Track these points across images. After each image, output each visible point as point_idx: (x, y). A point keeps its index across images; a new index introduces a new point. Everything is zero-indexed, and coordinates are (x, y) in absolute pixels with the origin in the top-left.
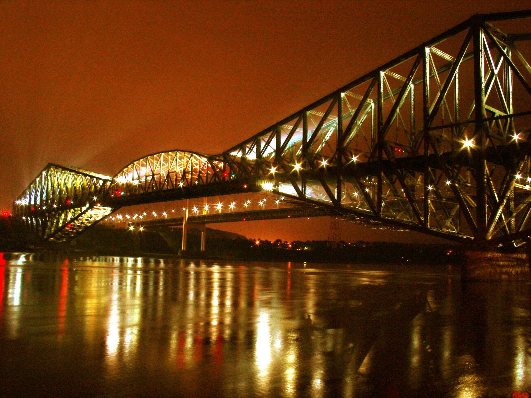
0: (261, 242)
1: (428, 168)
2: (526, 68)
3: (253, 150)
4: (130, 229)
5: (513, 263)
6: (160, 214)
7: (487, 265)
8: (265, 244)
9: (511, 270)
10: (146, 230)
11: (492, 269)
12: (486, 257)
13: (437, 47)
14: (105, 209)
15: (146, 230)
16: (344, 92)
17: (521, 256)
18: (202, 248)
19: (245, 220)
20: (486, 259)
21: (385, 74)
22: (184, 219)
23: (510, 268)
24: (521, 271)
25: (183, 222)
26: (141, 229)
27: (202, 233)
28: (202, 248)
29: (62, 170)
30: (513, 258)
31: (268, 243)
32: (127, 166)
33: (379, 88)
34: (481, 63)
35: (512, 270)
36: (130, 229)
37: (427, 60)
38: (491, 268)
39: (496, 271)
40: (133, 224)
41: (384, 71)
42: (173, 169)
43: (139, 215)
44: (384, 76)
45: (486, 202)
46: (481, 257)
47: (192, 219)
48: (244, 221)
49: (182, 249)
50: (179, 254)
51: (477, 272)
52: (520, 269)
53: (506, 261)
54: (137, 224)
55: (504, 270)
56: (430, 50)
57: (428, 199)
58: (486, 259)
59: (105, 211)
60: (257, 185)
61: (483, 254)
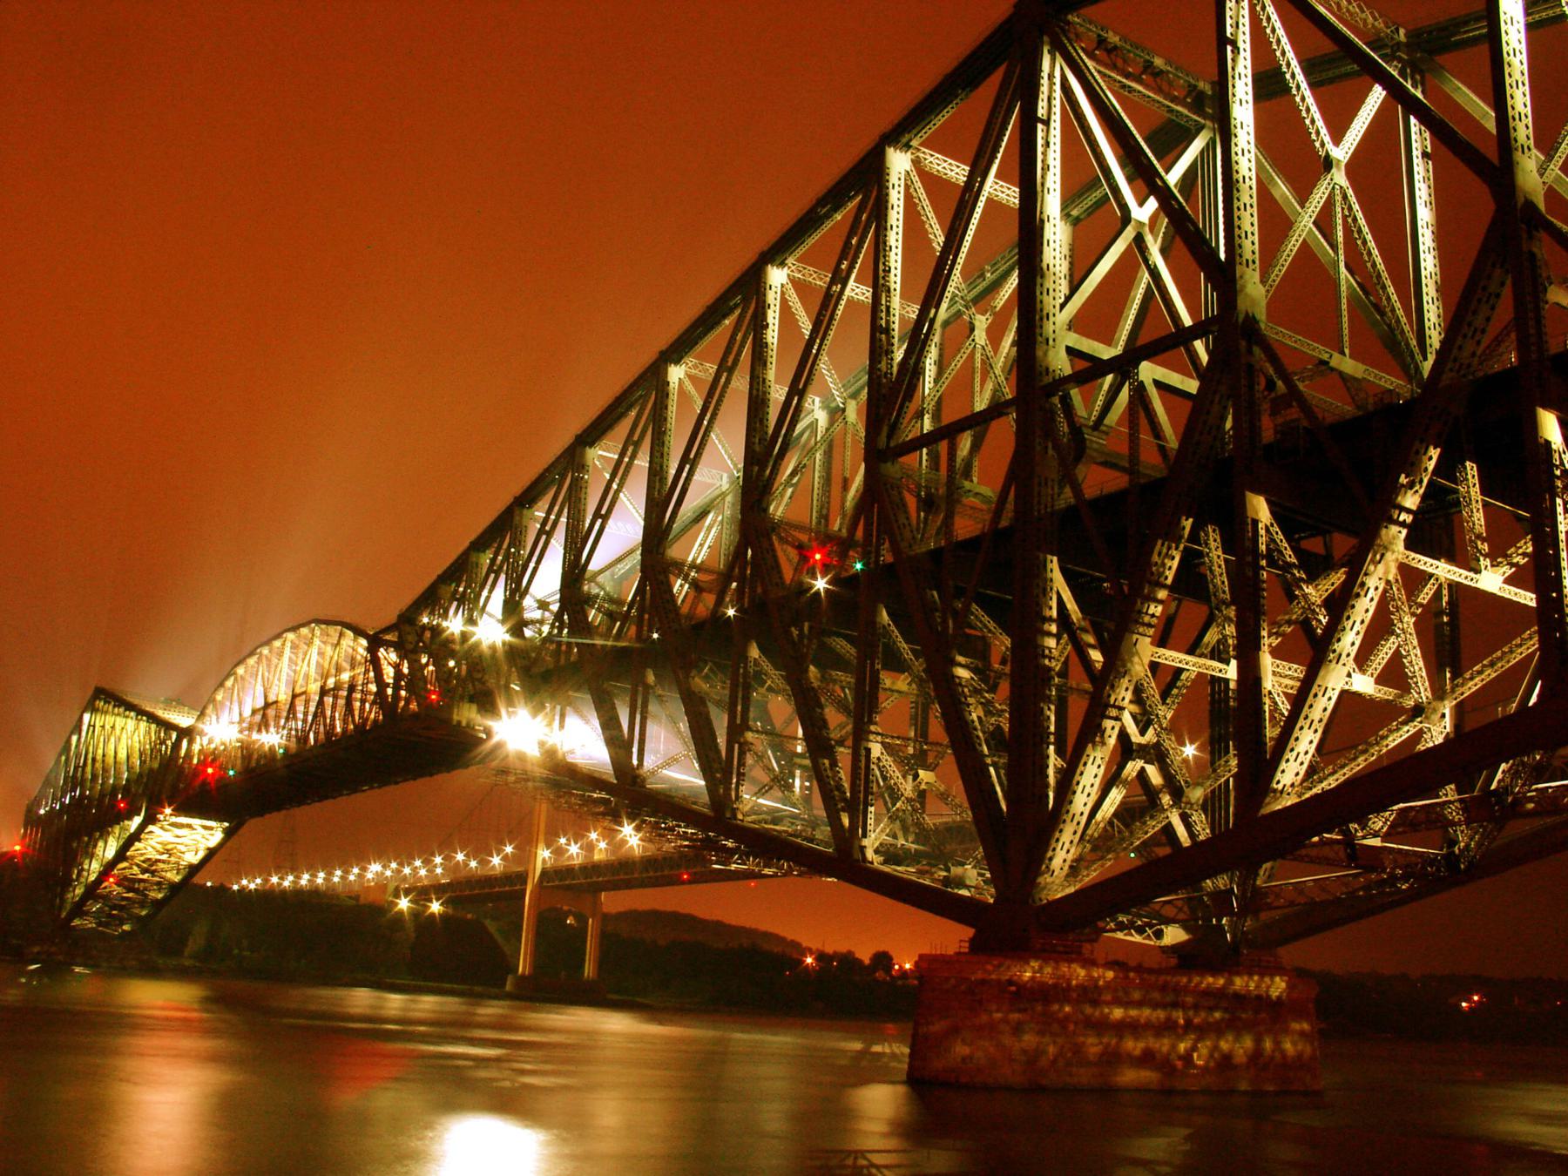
0: (821, 957)
1: (874, 613)
2: (1272, 195)
3: (488, 608)
4: (400, 907)
5: (1203, 1014)
6: (483, 862)
7: (1015, 1016)
8: (841, 967)
9: (1182, 1047)
10: (450, 911)
11: (1047, 1039)
12: (1010, 982)
13: (932, 144)
14: (205, 828)
15: (450, 911)
16: (677, 362)
17: (1252, 986)
18: (589, 970)
19: (690, 882)
20: (1013, 988)
21: (792, 280)
22: (531, 875)
23: (1181, 1038)
24: (1256, 1054)
25: (526, 883)
26: (436, 907)
27: (590, 920)
28: (589, 970)
29: (126, 710)
30: (1208, 993)
31: (848, 961)
32: (221, 685)
33: (759, 324)
34: (1046, 168)
35: (1194, 1048)
36: (400, 907)
37: (896, 198)
38: (1041, 1033)
39: (1078, 1050)
40: (407, 892)
41: (782, 264)
42: (302, 686)
43: (401, 864)
44: (782, 286)
45: (1052, 739)
46: (983, 982)
47: (557, 877)
48: (683, 882)
49: (586, 974)
50: (508, 987)
51: (961, 1050)
52: (1248, 1042)
53: (1155, 1006)
54: (422, 894)
55: (1133, 1046)
56: (916, 163)
57: (872, 737)
58: (1013, 988)
59: (207, 832)
60: (459, 723)
61: (989, 967)
